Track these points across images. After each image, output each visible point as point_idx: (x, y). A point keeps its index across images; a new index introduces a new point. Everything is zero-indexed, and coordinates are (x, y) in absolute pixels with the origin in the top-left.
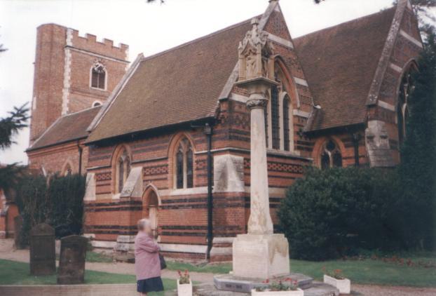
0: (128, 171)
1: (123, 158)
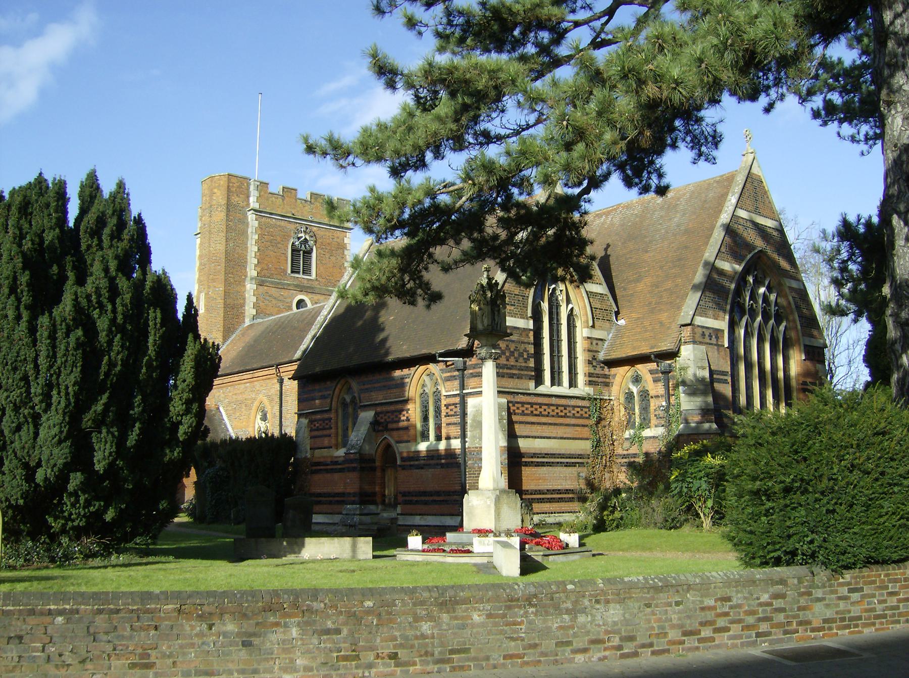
0: (355, 418)
1: (348, 399)
